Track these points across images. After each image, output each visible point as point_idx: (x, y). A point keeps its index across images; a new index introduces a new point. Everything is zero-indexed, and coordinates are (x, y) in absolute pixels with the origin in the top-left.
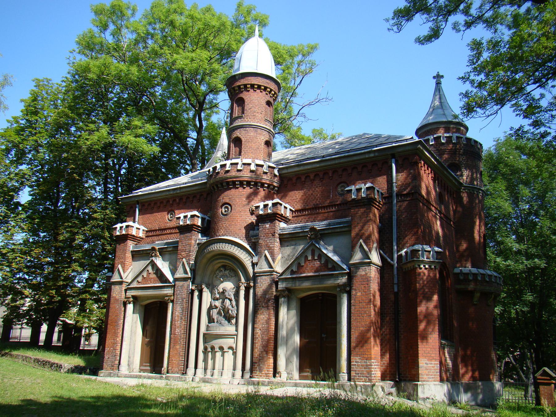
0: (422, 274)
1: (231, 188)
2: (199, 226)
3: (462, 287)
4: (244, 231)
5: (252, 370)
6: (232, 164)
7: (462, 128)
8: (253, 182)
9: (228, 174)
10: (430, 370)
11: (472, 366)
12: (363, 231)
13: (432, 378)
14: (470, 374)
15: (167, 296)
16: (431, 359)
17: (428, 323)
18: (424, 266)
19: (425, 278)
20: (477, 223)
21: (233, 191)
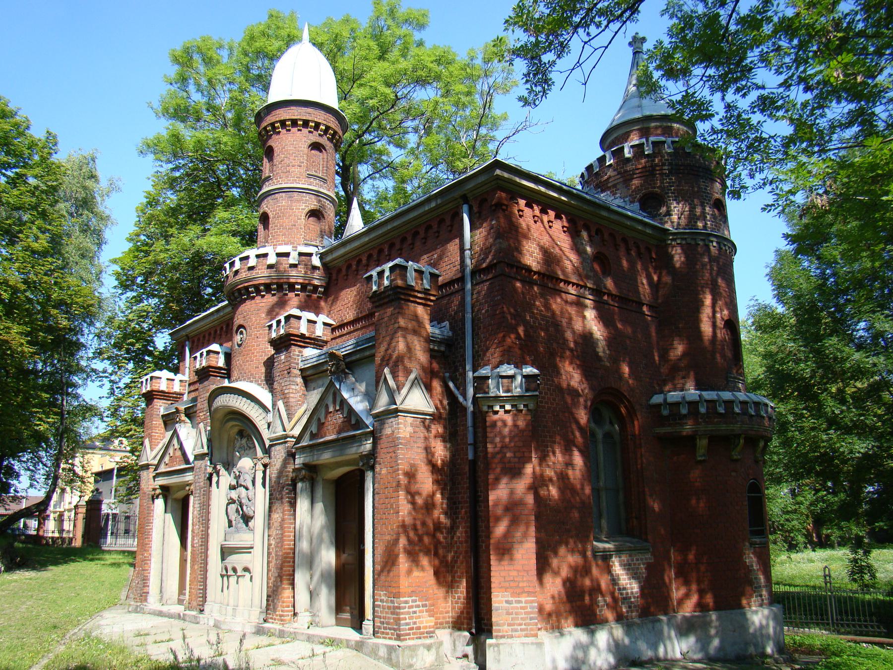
0: (499, 424)
1: (245, 300)
2: (220, 368)
3: (668, 429)
4: (263, 370)
6: (258, 256)
7: (675, 125)
8: (274, 284)
9: (237, 278)
10: (517, 614)
11: (699, 582)
12: (390, 351)
13: (522, 630)
14: (694, 599)
15: (188, 485)
16: (518, 592)
17: (515, 521)
18: (502, 407)
19: (506, 431)
20: (708, 300)
21: (248, 303)
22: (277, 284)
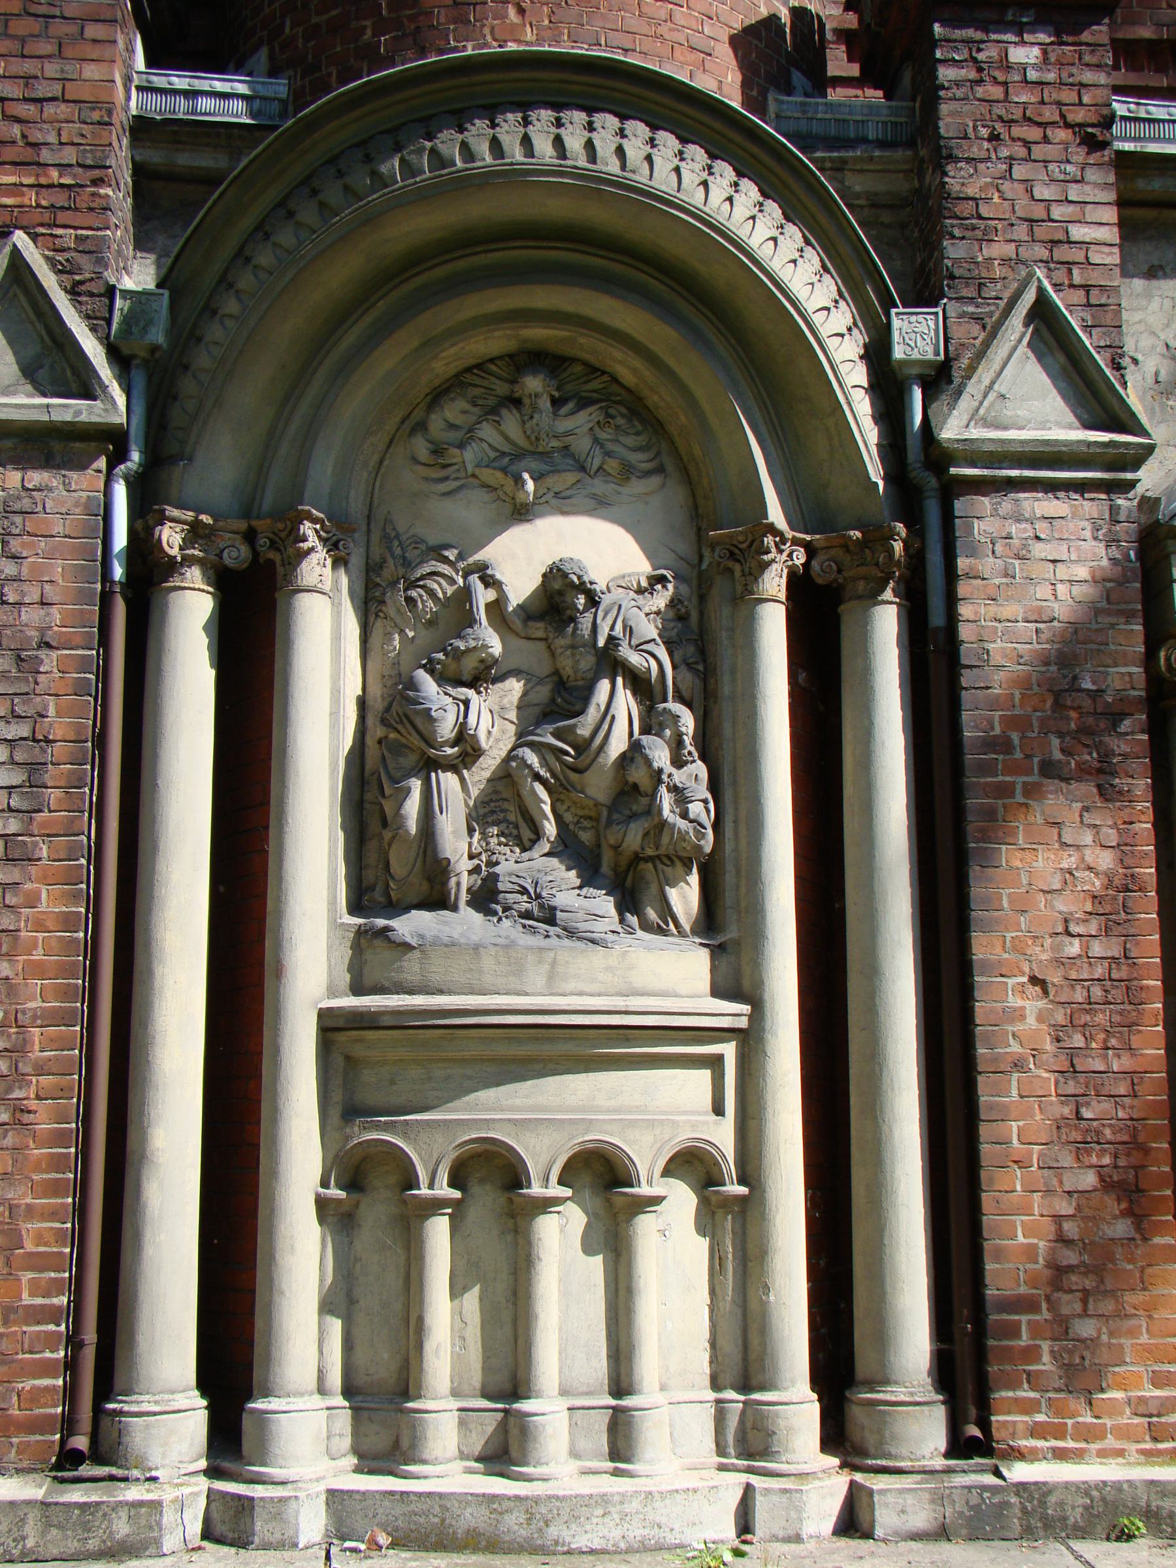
5: (965, 1377)
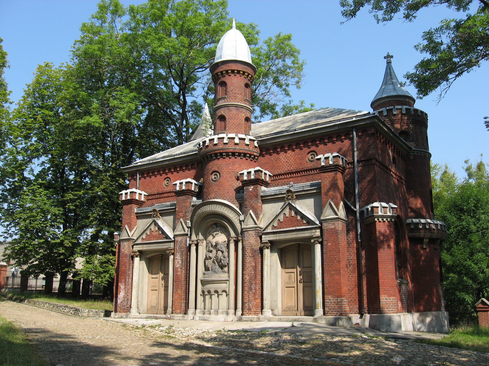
1: (214, 159)
10: (389, 304)
13: (391, 310)
21: (216, 160)
22: (238, 153)
